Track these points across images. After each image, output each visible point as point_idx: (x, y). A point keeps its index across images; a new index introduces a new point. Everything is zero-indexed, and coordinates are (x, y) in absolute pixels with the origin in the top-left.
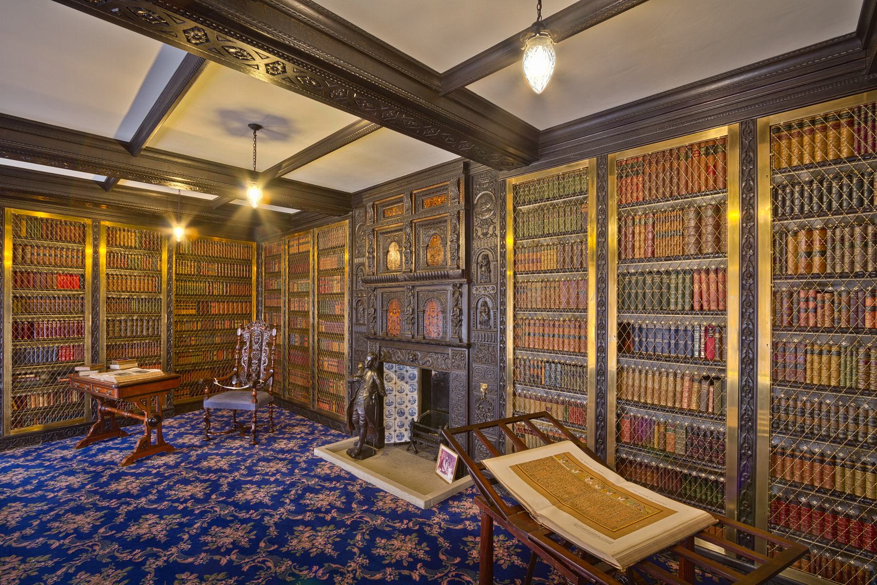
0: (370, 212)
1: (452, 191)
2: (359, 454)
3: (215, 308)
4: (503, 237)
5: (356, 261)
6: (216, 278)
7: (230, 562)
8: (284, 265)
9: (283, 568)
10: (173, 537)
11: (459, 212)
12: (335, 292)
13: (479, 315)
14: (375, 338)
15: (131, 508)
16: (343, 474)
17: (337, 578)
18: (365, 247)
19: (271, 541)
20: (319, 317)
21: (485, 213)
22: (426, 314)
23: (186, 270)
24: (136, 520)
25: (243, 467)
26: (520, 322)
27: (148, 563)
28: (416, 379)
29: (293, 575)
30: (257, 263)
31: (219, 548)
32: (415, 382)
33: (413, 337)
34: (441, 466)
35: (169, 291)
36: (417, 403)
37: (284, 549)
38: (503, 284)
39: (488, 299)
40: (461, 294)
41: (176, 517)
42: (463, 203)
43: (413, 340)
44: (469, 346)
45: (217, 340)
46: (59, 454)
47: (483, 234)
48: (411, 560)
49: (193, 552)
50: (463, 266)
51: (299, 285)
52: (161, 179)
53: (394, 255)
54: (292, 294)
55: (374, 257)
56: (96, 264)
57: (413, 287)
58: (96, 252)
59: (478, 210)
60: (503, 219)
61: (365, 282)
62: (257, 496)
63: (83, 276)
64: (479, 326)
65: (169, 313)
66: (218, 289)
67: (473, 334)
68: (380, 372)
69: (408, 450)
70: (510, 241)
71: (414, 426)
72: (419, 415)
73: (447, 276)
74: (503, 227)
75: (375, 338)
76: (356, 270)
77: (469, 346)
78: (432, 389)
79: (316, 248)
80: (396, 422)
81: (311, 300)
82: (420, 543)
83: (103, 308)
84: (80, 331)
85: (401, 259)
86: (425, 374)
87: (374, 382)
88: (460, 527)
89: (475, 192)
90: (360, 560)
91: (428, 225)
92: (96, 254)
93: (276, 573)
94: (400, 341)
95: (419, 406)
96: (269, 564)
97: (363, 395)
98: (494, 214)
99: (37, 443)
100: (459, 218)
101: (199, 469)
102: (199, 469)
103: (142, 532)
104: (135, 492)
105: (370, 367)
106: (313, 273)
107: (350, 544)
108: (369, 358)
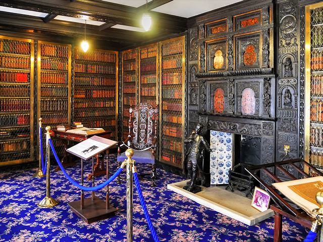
0: (202, 31)
1: (264, 15)
2: (195, 190)
3: (95, 94)
4: (303, 46)
5: (190, 63)
6: (96, 75)
7: (47, 227)
8: (137, 66)
9: (72, 233)
10: (23, 214)
11: (269, 30)
12: (174, 83)
13: (283, 98)
14: (205, 114)
15: (5, 199)
16: (190, 201)
17: (97, 240)
18: (197, 53)
19: (69, 220)
20: (163, 99)
21: (288, 29)
22: (243, 98)
23: (79, 70)
24: (7, 205)
25: (64, 185)
26: (315, 104)
27: (9, 224)
28: (231, 142)
29: (76, 236)
30: (119, 65)
31: (43, 221)
32: (231, 144)
33: (234, 114)
34: (256, 201)
35: (72, 83)
36: (231, 158)
37: (74, 225)
38: (303, 78)
39: (289, 88)
40: (270, 85)
41: (26, 205)
42: (272, 23)
43: (234, 116)
44: (276, 120)
45: (97, 114)
46: (23, 179)
47: (286, 44)
48: (139, 237)
49: (31, 221)
50: (272, 66)
51: (149, 79)
52: (73, 13)
53: (219, 60)
54: (143, 85)
55: (204, 60)
56: (35, 67)
57: (234, 80)
58: (36, 59)
59: (282, 27)
60: (303, 33)
61: (198, 76)
62: (68, 199)
63: (29, 74)
64: (283, 106)
65: (72, 97)
66: (97, 82)
67: (279, 112)
68: (207, 137)
69: (226, 189)
70: (308, 47)
71: (231, 174)
72: (233, 167)
73: (260, 73)
74: (303, 39)
75: (205, 114)
76: (190, 69)
77: (276, 120)
78: (243, 151)
79: (160, 54)
80: (218, 170)
81: (157, 89)
82: (147, 230)
83: (39, 93)
84: (28, 106)
85: (225, 61)
86: (237, 138)
87: (201, 143)
88: (173, 224)
89: (280, 15)
90: (112, 234)
91: (243, 39)
92: (35, 61)
93: (68, 234)
94: (223, 116)
95: (233, 160)
96: (65, 230)
97: (195, 151)
98: (295, 30)
99: (9, 171)
100: (269, 33)
101: (41, 184)
102: (41, 184)
103: (8, 210)
104: (9, 192)
105: (199, 133)
106: (159, 71)
107: (109, 226)
108: (198, 127)
